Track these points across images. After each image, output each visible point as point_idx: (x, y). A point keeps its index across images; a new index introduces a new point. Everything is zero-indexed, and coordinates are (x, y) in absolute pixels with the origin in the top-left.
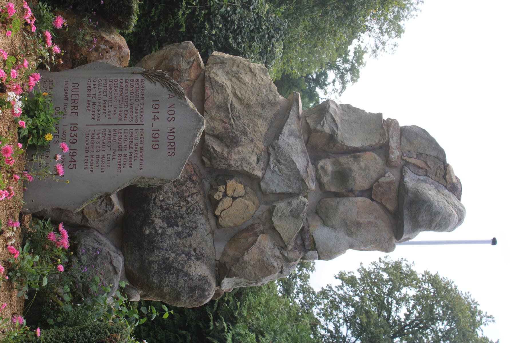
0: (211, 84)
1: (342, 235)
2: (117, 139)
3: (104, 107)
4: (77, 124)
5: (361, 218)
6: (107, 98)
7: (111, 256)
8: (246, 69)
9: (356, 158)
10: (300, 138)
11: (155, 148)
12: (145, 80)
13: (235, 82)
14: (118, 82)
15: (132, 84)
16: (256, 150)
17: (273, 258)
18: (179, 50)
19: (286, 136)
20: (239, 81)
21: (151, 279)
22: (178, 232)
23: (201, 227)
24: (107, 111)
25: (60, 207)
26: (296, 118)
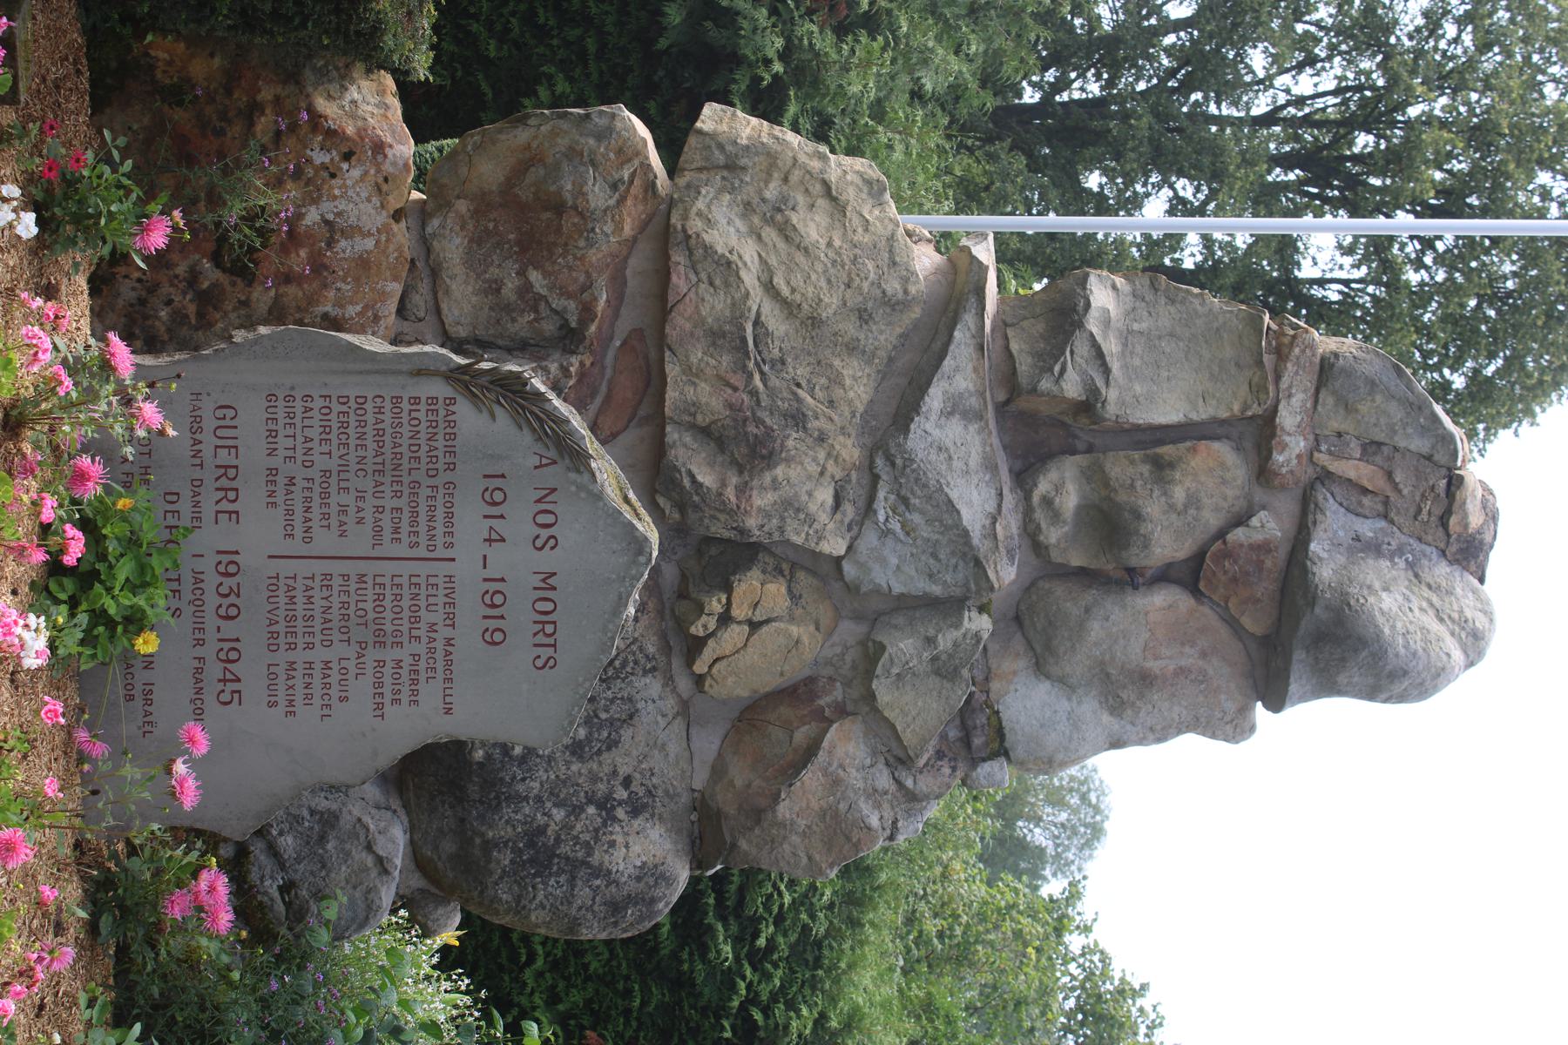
0: (691, 254)
1: (1089, 707)
2: (369, 606)
3: (325, 495)
4: (237, 553)
5: (1156, 658)
6: (333, 464)
7: (368, 830)
8: (811, 188)
9: (1161, 468)
10: (981, 418)
11: (493, 638)
12: (459, 399)
13: (770, 243)
14: (369, 406)
15: (414, 414)
16: (831, 467)
17: (868, 797)
18: (582, 141)
19: (933, 417)
20: (787, 239)
21: (491, 892)
22: (574, 742)
23: (649, 715)
24: (334, 509)
25: (198, 826)
26: (971, 349)
